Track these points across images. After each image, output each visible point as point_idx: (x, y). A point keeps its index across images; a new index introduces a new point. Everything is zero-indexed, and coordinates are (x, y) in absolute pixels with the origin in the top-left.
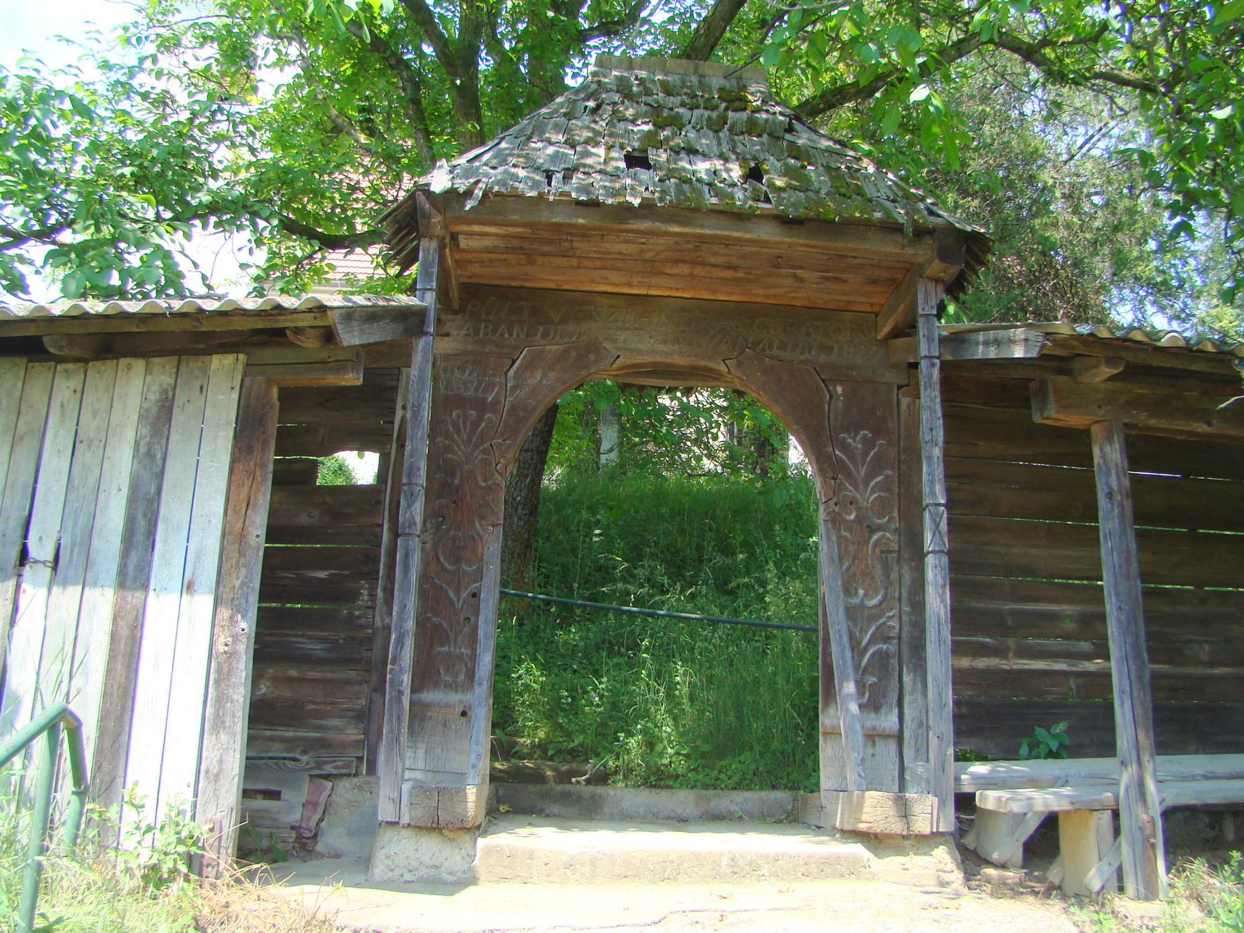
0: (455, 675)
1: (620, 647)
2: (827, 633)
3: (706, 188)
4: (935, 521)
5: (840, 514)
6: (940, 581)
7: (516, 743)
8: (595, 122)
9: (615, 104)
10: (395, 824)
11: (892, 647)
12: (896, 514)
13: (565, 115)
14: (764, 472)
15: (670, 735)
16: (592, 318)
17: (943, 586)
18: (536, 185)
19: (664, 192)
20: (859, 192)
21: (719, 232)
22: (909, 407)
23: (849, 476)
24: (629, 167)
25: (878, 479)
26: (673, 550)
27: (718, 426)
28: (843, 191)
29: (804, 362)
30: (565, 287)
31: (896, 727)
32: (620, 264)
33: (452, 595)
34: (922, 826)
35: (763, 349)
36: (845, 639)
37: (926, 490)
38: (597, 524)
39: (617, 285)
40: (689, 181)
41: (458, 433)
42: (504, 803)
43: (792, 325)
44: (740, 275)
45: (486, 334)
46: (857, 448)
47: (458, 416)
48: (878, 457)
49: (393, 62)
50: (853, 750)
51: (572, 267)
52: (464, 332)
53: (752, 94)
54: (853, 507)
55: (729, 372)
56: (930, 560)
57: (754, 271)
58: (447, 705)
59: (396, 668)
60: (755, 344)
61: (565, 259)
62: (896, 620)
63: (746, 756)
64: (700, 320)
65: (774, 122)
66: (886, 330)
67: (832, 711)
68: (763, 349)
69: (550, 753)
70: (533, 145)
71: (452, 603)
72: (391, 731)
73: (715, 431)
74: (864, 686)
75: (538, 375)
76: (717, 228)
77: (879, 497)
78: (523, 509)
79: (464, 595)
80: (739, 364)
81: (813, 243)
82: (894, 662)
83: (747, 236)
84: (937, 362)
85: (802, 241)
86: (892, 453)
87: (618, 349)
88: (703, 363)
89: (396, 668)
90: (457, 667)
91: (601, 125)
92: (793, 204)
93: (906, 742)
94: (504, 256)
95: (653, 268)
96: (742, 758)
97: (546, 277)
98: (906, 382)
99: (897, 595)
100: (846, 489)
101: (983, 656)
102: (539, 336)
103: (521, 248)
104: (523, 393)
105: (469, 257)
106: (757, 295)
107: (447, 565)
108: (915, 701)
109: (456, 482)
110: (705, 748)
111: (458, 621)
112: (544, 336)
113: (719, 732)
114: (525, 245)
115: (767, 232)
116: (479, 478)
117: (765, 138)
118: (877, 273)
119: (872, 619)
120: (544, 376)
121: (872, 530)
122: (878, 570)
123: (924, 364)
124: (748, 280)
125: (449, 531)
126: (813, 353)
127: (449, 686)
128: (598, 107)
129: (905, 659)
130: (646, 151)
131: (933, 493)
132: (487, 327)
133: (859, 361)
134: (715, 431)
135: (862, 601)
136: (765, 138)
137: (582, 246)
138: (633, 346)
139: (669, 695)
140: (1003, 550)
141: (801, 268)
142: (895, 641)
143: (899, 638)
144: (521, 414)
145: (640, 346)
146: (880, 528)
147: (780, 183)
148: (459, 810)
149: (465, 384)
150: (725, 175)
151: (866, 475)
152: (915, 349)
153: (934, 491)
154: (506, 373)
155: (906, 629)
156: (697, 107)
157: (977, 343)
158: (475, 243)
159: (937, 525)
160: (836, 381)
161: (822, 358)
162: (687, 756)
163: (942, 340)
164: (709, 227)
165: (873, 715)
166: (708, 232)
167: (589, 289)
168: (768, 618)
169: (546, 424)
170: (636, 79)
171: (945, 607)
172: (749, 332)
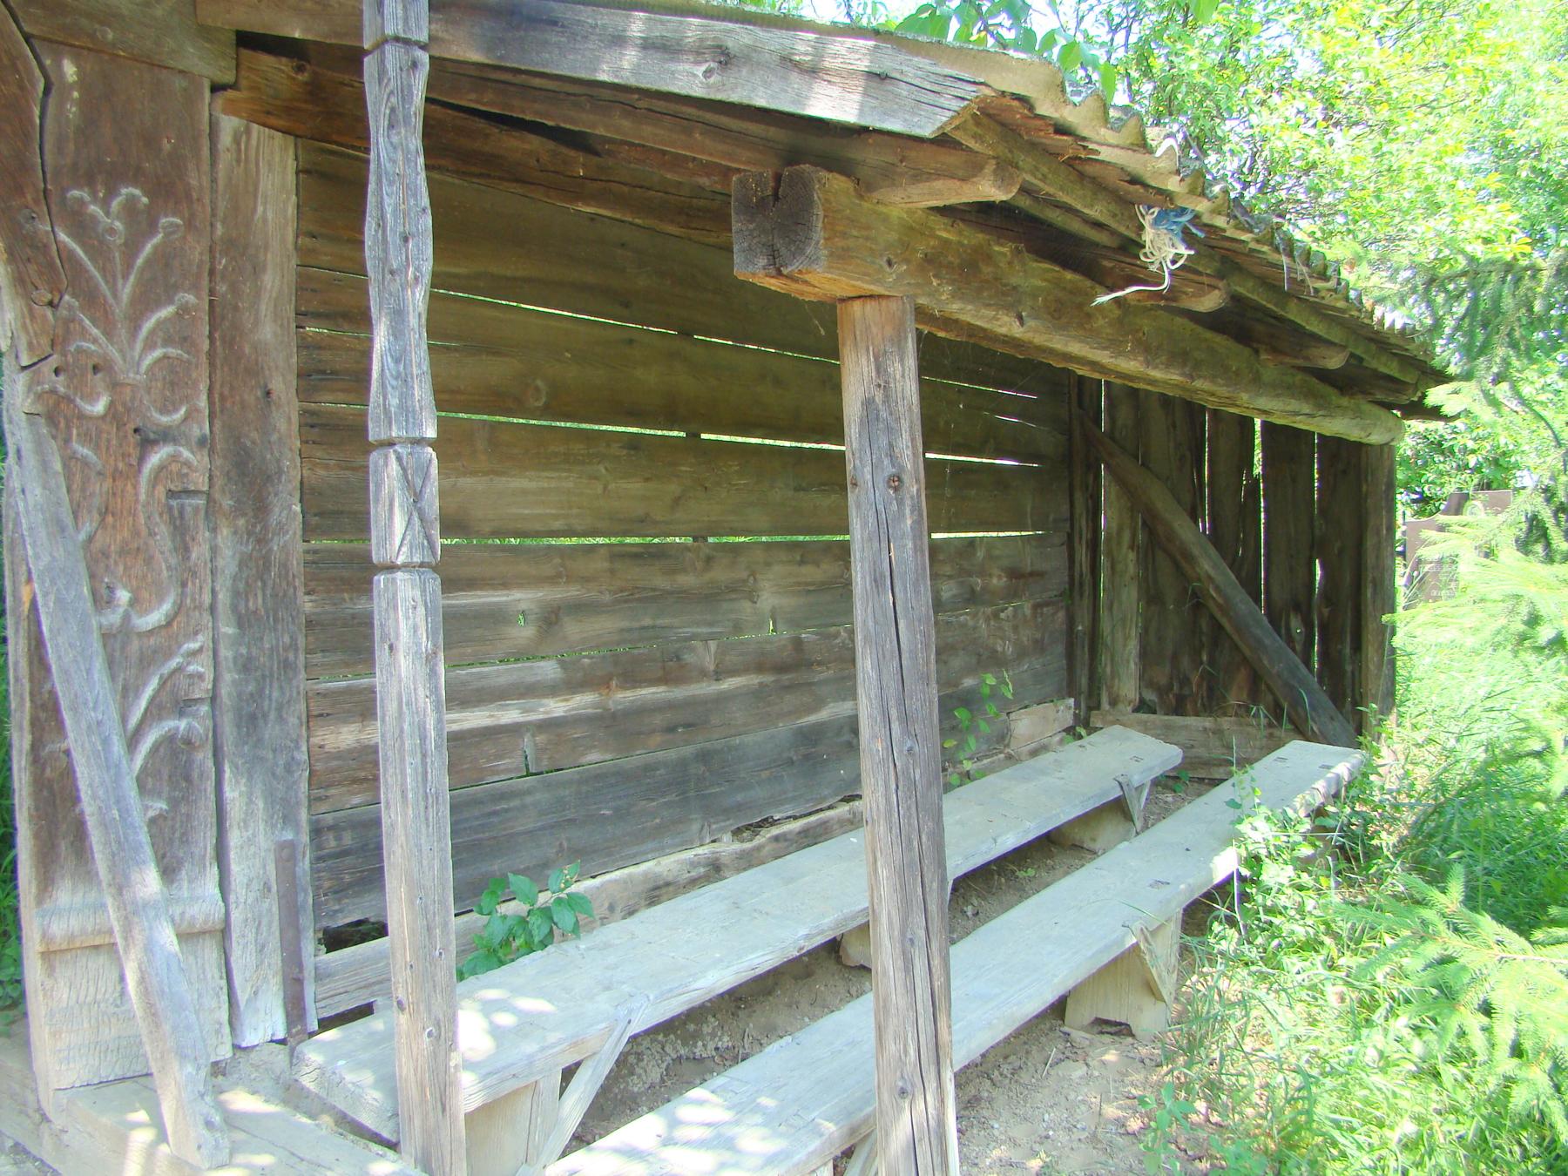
6: (425, 644)
12: (203, 402)
23: (91, 299)
46: (112, 231)
48: (163, 259)
62: (207, 657)
67: (64, 895)
77: (166, 357)
84: (424, 57)
86: (196, 251)
98: (229, 77)
99: (207, 598)
100: (84, 333)
119: (147, 662)
121: (147, 442)
129: (228, 748)
135: (126, 618)
142: (204, 709)
143: (214, 699)
146: (166, 436)
151: (134, 301)
155: (228, 677)
159: (417, 497)
160: (60, 45)
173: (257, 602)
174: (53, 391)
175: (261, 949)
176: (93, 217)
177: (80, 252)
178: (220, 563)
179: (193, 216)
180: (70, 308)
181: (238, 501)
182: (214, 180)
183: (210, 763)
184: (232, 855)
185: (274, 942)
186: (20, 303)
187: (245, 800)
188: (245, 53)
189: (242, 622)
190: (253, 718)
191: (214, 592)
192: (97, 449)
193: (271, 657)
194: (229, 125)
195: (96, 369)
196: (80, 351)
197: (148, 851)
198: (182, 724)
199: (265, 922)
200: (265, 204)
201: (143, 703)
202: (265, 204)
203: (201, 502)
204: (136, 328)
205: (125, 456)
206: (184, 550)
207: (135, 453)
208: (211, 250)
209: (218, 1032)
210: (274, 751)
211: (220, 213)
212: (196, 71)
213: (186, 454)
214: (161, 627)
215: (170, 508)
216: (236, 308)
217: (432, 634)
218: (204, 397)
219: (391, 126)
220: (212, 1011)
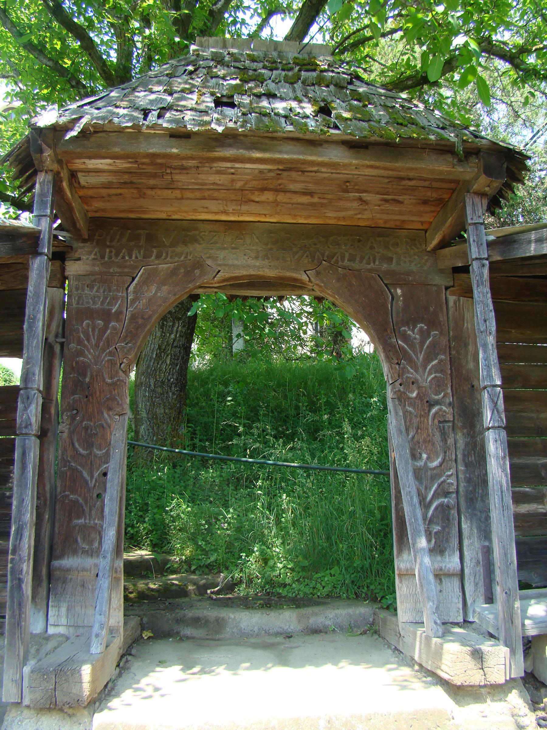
0: (91, 542)
1: (243, 482)
2: (398, 492)
3: (283, 120)
4: (493, 401)
5: (405, 393)
6: (501, 454)
7: (169, 561)
8: (192, 79)
9: (209, 67)
10: (18, 704)
11: (451, 500)
12: (449, 391)
13: (167, 75)
14: (339, 355)
15: (278, 553)
16: (196, 241)
17: (504, 458)
18: (132, 118)
19: (245, 122)
20: (413, 123)
21: (295, 157)
22: (455, 303)
23: (410, 361)
24: (216, 107)
25: (434, 363)
26: (279, 410)
27: (306, 324)
28: (400, 121)
29: (370, 271)
30: (174, 217)
31: (459, 567)
32: (216, 194)
33: (85, 475)
34: (498, 676)
35: (337, 262)
36: (416, 500)
37: (482, 372)
38: (229, 393)
39: (216, 213)
40: (265, 115)
41: (88, 340)
42: (148, 629)
43: (359, 241)
44: (315, 200)
45: (110, 257)
46: (415, 338)
47: (88, 325)
48: (433, 345)
49: (74, 83)
50: (429, 599)
51: (177, 199)
52: (93, 256)
53: (320, 61)
54: (414, 387)
55: (310, 281)
56: (490, 436)
57: (326, 196)
58: (84, 570)
59: (17, 557)
60: (330, 257)
61: (170, 191)
62: (454, 477)
63: (335, 570)
64: (285, 239)
65: (339, 78)
66: (435, 242)
67: (405, 556)
68: (337, 262)
69: (193, 568)
70: (137, 94)
71: (86, 482)
72: (13, 616)
73: (305, 328)
74: (430, 534)
75: (153, 289)
76: (293, 153)
77: (435, 377)
78: (175, 387)
79: (96, 475)
80: (318, 274)
81: (377, 164)
82: (454, 513)
83: (320, 159)
84: (487, 262)
85: (367, 163)
86: (444, 341)
87: (220, 265)
88: (288, 274)
89: (17, 557)
90: (93, 535)
91: (197, 81)
92: (359, 131)
93: (466, 578)
94: (119, 191)
95: (243, 195)
96: (333, 572)
97: (158, 208)
98: (451, 284)
99: (454, 457)
100: (409, 372)
101: (524, 503)
102: (153, 258)
103: (132, 183)
104: (141, 304)
105: (90, 193)
106: (330, 218)
107: (81, 450)
108: (472, 544)
109: (87, 380)
110: (306, 563)
111: (91, 498)
112: (158, 257)
113: (314, 550)
114: (134, 179)
115: (337, 155)
116: (106, 376)
117: (332, 87)
118: (429, 194)
119: (433, 478)
120: (159, 289)
121: (431, 405)
122: (437, 437)
123: (475, 265)
124: (322, 205)
125: (82, 422)
126: (377, 263)
127: (85, 552)
128: (196, 70)
129: (463, 509)
130: (233, 96)
131: (490, 376)
132: (111, 252)
133: (413, 268)
134: (305, 328)
135: (426, 463)
136: (332, 87)
137: (182, 178)
138: (230, 262)
139: (278, 522)
140: (534, 415)
141: (365, 191)
142: (454, 495)
143: (457, 492)
144: (140, 321)
145: (236, 262)
146: (437, 403)
147: (346, 115)
148: (74, 691)
149: (93, 298)
150: (298, 110)
151: (424, 359)
152: (465, 255)
153: (490, 373)
154: (127, 289)
155: (462, 485)
156: (277, 69)
157: (530, 242)
158: (93, 180)
159: (495, 404)
160: (396, 285)
161: (385, 267)
162: (292, 570)
163: (490, 244)
164: (287, 153)
165: (439, 558)
166: (286, 156)
167: (194, 218)
168: (348, 465)
169: (188, 329)
170: (229, 54)
171: (506, 476)
172: (325, 251)
173: (472, 458)
174: (399, 391)
175: (476, 585)
176: (409, 335)
177: (406, 346)
178: (458, 445)
179: (442, 330)
180: (403, 364)
181: (464, 423)
182: (448, 318)
183: (456, 515)
184: (465, 548)
185: (481, 583)
186: (388, 364)
187: (469, 529)
188: (456, 275)
189: (466, 465)
190: (472, 499)
191: (456, 455)
192: (414, 408)
193: (478, 478)
194: (452, 299)
195: (413, 383)
196: (407, 377)
197: (423, 533)
198: (446, 500)
199: (477, 575)
200: (467, 323)
201: (432, 492)
202: (467, 323)
203: (451, 424)
204: (426, 368)
205: (424, 410)
206: (445, 440)
207: (427, 409)
208: (449, 340)
209: (458, 611)
210: (481, 512)
211: (451, 328)
212: (439, 284)
213: (444, 408)
214: (437, 467)
215: (440, 427)
216: (459, 358)
217: (503, 451)
218: (450, 389)
219: (478, 286)
220: (456, 603)
